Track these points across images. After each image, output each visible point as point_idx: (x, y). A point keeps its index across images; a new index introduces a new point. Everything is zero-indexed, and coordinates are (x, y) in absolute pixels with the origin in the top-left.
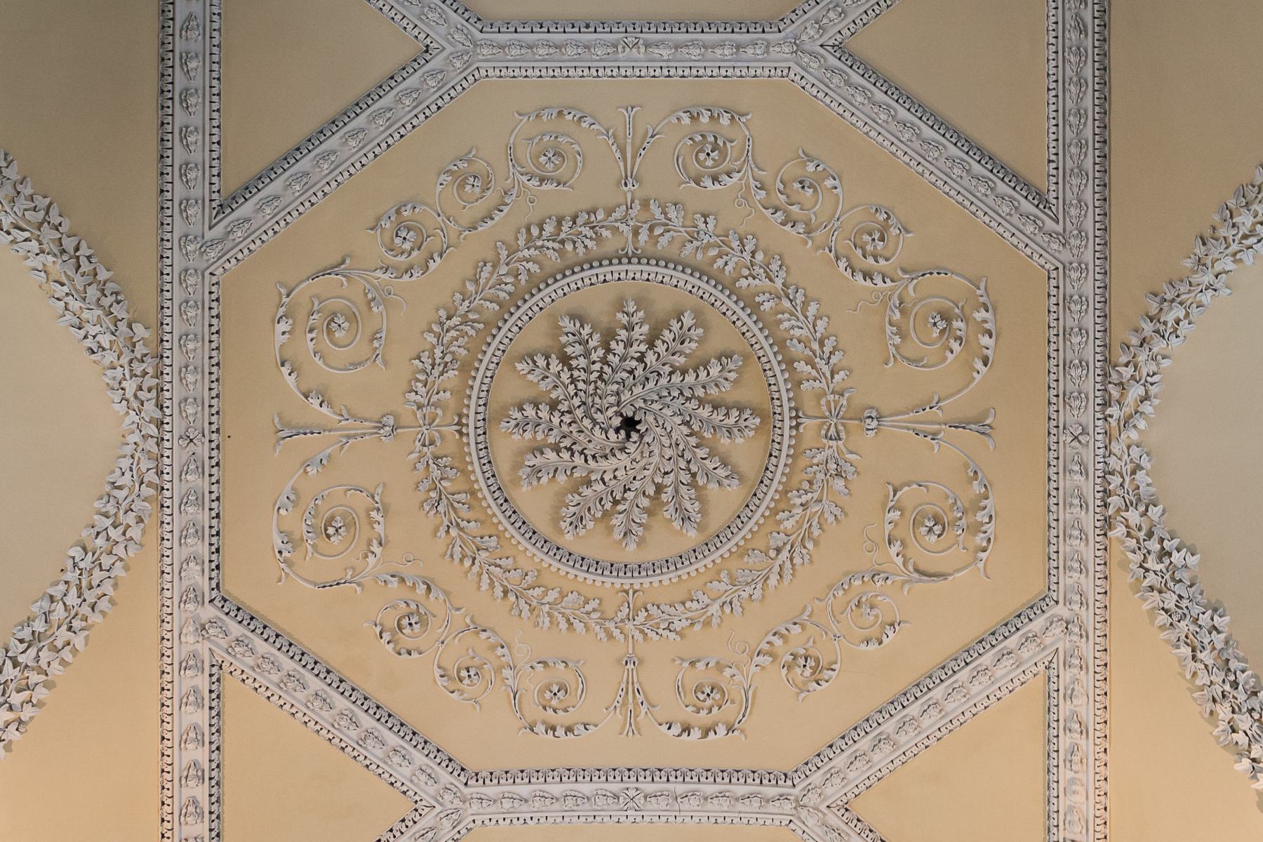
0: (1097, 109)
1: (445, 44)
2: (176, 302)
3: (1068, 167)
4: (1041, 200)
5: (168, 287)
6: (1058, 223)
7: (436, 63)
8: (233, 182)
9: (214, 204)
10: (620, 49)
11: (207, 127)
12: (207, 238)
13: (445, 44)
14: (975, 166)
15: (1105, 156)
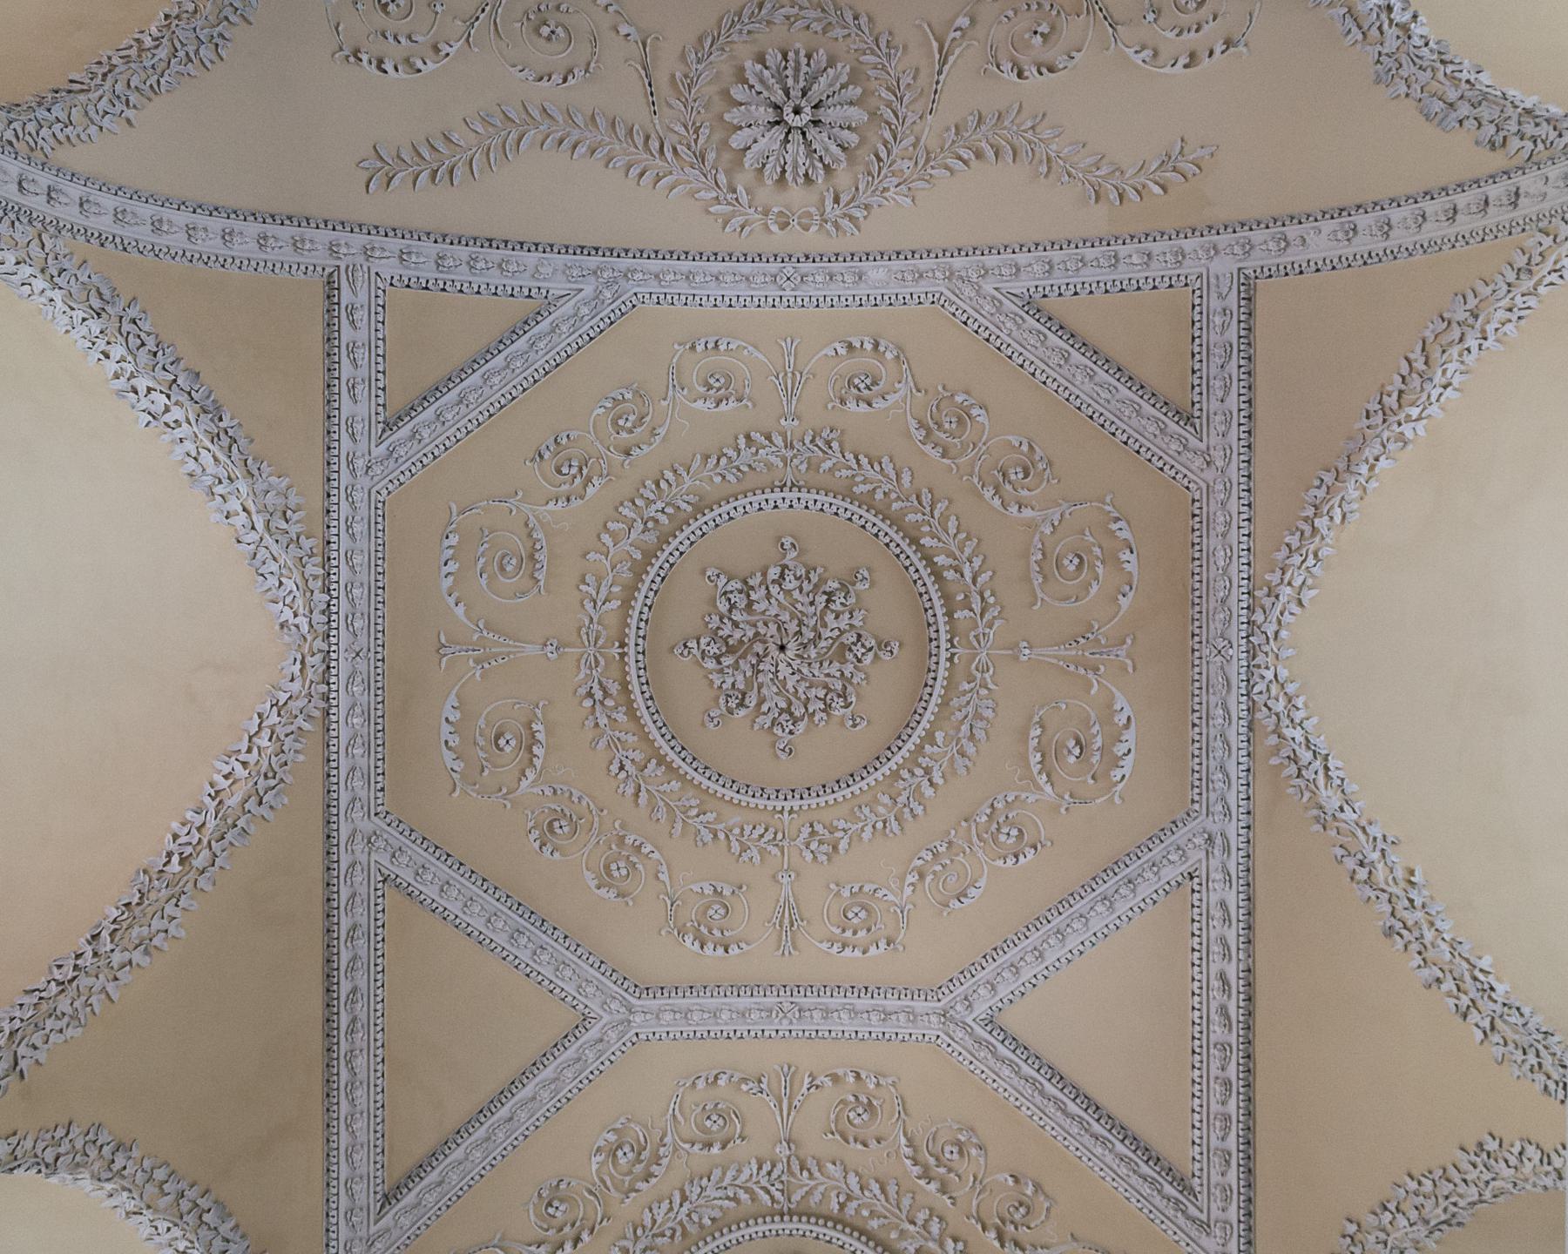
0: (1241, 1083)
1: (601, 1013)
2: (342, 1211)
3: (1211, 608)
4: (1182, 1183)
5: (334, 757)
6: (1202, 1211)
7: (594, 1033)
8: (398, 402)
9: (379, 1197)
10: (774, 1015)
11: (372, 898)
12: (373, 455)
13: (601, 1013)
14: (1119, 1146)
15: (1249, 1085)
